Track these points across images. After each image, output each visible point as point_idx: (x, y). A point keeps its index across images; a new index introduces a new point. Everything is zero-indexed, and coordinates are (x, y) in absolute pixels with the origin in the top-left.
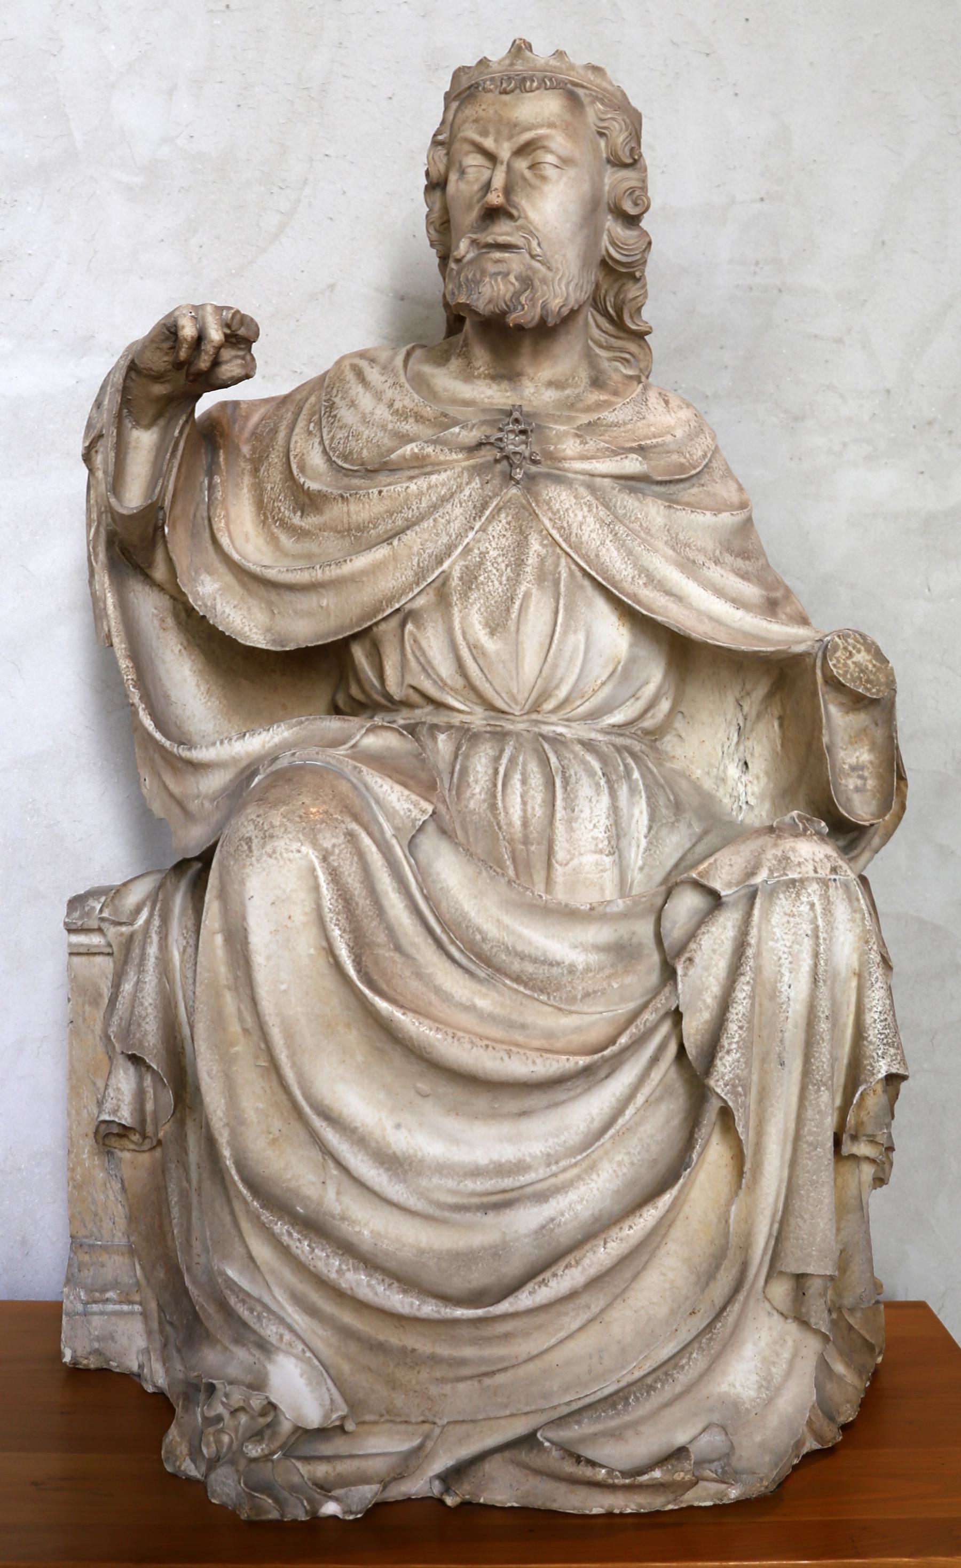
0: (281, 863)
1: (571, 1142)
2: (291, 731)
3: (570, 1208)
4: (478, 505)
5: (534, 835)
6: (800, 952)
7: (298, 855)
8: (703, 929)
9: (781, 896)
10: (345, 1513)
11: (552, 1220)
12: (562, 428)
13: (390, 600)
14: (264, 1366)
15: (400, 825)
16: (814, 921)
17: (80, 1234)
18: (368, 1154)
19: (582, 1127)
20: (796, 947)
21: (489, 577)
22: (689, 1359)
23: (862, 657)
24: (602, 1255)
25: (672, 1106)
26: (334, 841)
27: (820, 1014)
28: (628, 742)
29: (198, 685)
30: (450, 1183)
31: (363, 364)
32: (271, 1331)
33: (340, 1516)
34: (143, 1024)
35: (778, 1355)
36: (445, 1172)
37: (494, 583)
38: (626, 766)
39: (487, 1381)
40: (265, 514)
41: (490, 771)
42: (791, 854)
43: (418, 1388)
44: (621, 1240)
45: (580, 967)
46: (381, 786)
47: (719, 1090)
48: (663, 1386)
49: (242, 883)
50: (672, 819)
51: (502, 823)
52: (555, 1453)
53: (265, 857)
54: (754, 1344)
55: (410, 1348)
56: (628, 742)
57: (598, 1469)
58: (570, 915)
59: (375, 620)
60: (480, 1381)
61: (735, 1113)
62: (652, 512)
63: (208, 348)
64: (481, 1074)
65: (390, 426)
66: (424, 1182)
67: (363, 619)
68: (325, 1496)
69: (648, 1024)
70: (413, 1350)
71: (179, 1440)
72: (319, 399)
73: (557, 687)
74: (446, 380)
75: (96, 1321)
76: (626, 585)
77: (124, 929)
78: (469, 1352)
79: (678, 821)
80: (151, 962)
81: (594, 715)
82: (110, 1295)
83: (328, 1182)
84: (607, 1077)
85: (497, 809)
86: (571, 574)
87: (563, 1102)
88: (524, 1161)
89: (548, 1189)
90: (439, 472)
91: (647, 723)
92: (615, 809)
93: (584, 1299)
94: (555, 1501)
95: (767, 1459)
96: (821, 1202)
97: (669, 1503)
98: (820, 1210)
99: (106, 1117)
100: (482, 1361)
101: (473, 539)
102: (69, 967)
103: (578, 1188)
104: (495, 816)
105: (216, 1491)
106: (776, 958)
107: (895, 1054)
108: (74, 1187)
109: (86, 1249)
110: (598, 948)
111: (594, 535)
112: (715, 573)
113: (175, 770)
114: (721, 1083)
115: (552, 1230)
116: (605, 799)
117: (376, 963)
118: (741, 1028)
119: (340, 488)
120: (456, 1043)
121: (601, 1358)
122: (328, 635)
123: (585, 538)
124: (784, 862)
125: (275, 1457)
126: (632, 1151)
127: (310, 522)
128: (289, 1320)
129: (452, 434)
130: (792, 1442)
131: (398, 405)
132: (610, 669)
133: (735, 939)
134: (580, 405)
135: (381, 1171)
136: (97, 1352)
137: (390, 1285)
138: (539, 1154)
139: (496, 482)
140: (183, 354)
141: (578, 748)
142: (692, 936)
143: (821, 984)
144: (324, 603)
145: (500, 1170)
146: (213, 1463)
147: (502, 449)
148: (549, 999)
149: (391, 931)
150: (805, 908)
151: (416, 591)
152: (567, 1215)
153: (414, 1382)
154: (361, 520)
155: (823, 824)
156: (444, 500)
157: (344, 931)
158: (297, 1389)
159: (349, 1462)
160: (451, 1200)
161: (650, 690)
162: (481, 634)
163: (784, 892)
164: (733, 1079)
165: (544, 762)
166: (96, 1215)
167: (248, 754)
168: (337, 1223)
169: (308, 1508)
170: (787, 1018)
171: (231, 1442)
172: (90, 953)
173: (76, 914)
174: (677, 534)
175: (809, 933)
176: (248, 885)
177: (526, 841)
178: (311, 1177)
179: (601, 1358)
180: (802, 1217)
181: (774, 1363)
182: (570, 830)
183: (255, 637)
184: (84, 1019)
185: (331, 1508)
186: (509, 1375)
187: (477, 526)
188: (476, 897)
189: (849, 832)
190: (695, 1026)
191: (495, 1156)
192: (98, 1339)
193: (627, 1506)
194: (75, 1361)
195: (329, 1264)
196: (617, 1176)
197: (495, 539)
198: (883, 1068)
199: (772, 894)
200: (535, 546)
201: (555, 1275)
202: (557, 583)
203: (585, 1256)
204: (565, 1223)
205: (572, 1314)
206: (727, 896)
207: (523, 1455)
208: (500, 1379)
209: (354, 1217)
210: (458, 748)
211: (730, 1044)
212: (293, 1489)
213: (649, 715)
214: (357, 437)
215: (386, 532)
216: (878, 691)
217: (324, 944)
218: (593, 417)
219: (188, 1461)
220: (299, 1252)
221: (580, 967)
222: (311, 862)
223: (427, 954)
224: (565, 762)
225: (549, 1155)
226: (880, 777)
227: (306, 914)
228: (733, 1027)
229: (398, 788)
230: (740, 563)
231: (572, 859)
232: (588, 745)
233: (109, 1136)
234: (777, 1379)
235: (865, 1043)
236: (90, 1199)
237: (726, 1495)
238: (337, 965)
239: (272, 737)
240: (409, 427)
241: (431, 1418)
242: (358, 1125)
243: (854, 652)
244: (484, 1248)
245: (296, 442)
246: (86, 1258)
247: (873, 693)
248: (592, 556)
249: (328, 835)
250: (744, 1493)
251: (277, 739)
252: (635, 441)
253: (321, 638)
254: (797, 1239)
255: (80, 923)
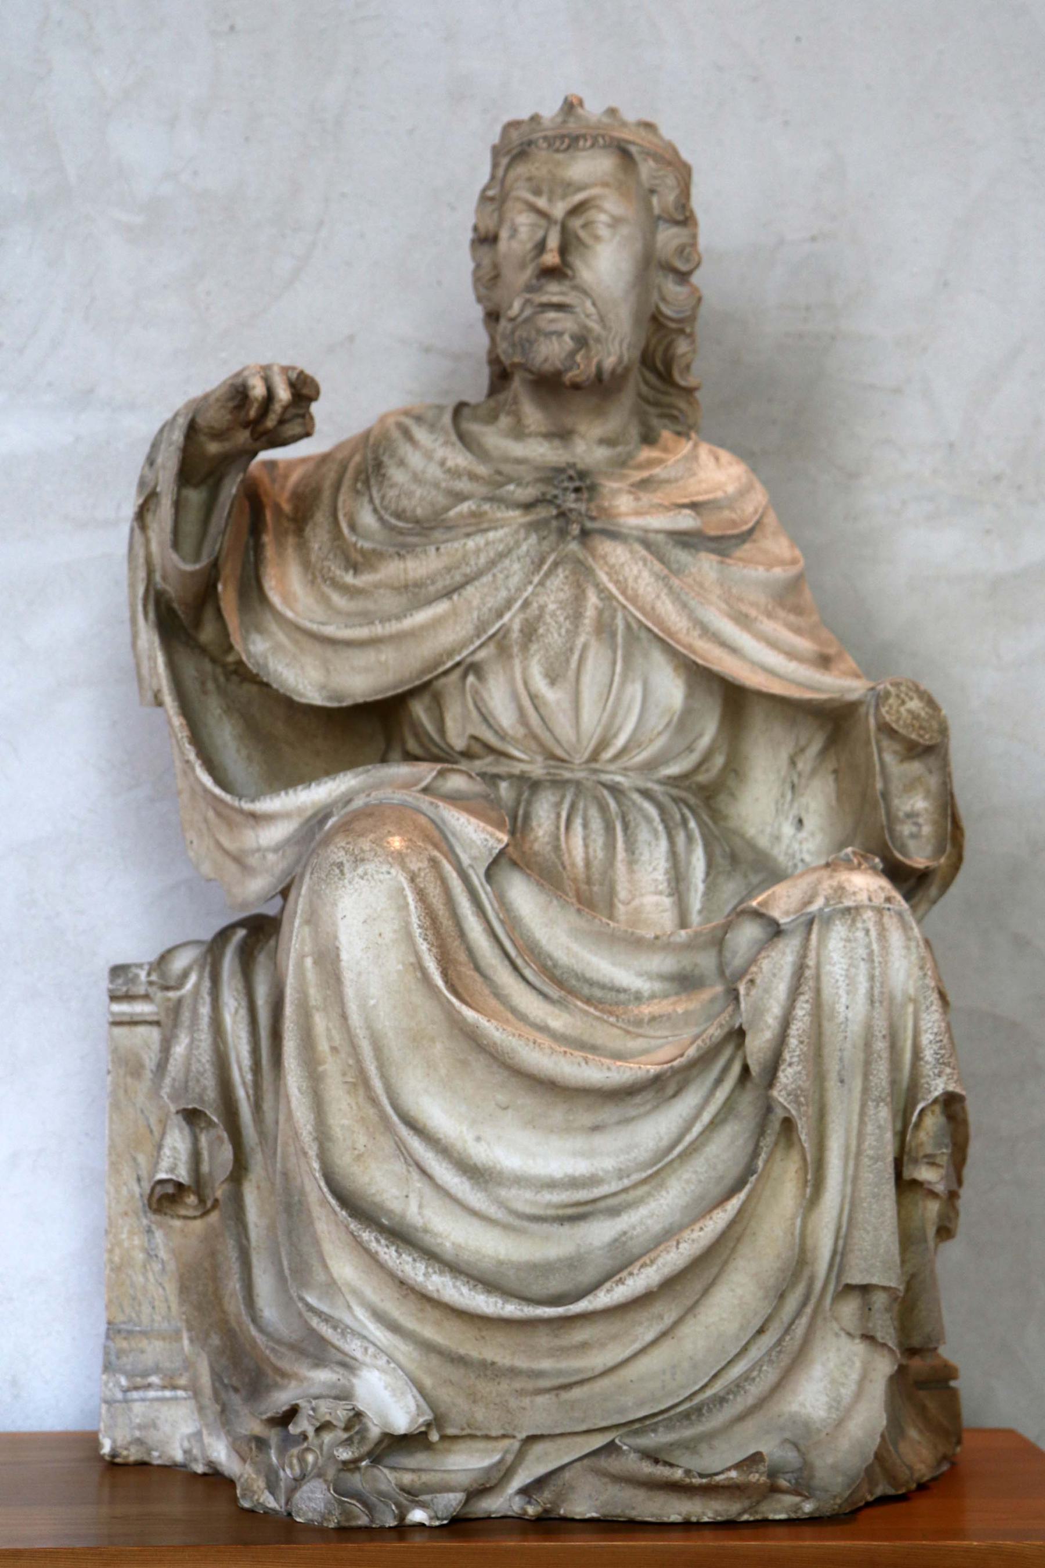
0: (373, 883)
1: (642, 1159)
2: (358, 779)
3: (641, 1223)
4: (536, 560)
5: (596, 876)
6: (857, 975)
7: (388, 876)
8: (763, 954)
9: (837, 922)
10: (431, 1518)
11: (625, 1233)
12: (615, 485)
13: (450, 654)
14: (349, 1380)
15: (478, 854)
16: (869, 946)
17: (117, 1321)
18: (451, 1163)
19: (651, 1145)
20: (853, 970)
21: (548, 630)
22: (760, 1371)
23: (915, 704)
24: (673, 1258)
25: (736, 1128)
26: (420, 865)
27: (877, 1033)
28: (683, 794)
29: (238, 751)
30: (529, 1195)
31: (408, 422)
32: (354, 1347)
33: (427, 1523)
34: (202, 1079)
35: (846, 1376)
36: (522, 1184)
37: (553, 636)
38: (683, 816)
39: (565, 1396)
40: (313, 574)
41: (553, 816)
42: (846, 885)
43: (498, 1400)
44: (693, 1241)
45: (646, 994)
46: (458, 819)
47: (781, 1100)
48: (735, 1397)
49: (335, 904)
50: (729, 868)
51: (567, 863)
52: (633, 1456)
53: (357, 879)
54: (823, 1365)
55: (489, 1361)
56: (683, 794)
57: (675, 1469)
58: (636, 944)
59: (435, 673)
60: (557, 1395)
61: (799, 1122)
62: (705, 566)
63: (277, 407)
64: (559, 1079)
65: (443, 485)
66: (503, 1193)
67: (423, 672)
68: (412, 1501)
69: (713, 1039)
70: (493, 1363)
71: (254, 1476)
72: (368, 462)
73: (615, 736)
74: (494, 438)
75: (138, 1408)
76: (682, 636)
77: (172, 995)
78: (546, 1364)
79: (734, 870)
80: (205, 1022)
81: (649, 766)
82: (154, 1379)
83: (411, 1195)
84: (675, 1095)
85: (560, 850)
86: (628, 627)
87: (633, 1119)
88: (597, 1175)
89: (620, 1204)
90: (495, 528)
91: (702, 778)
92: (673, 853)
93: (658, 1307)
94: (633, 1508)
95: (840, 1479)
96: (883, 1214)
97: (744, 1512)
98: (883, 1223)
99: (162, 1176)
100: (560, 1373)
101: (533, 593)
102: (111, 1038)
103: (648, 1203)
104: (559, 857)
105: (301, 1509)
106: (833, 981)
107: (952, 1074)
108: (112, 1270)
109: (124, 1335)
110: (662, 977)
111: (649, 589)
112: (768, 626)
113: (230, 824)
114: (783, 1093)
115: (624, 1243)
116: (664, 844)
117: (460, 978)
118: (802, 1042)
119: (395, 545)
120: (537, 1049)
121: (674, 1374)
122: (388, 689)
123: (641, 591)
124: (840, 892)
125: (364, 1463)
126: (699, 1169)
127: (364, 580)
128: (372, 1338)
129: (508, 492)
130: (864, 1466)
131: (450, 463)
132: (666, 720)
133: (794, 963)
134: (632, 463)
135: (464, 1179)
136: (139, 1442)
137: (475, 1286)
138: (610, 1168)
139: (553, 538)
140: (253, 413)
141: (636, 796)
142: (753, 961)
143: (877, 1005)
144: (383, 658)
145: (574, 1183)
146: (292, 1491)
147: (558, 506)
148: (618, 1021)
149: (470, 952)
150: (860, 934)
151: (478, 643)
152: (638, 1230)
153: (494, 1394)
154: (418, 576)
155: (877, 860)
156: (502, 556)
157: (433, 945)
158: (389, 1401)
159: (433, 1473)
160: (529, 1210)
161: (705, 741)
162: (540, 684)
163: (840, 919)
164: (795, 1090)
165: (603, 809)
166: (134, 1299)
167: (313, 804)
168: (420, 1235)
169: (396, 1512)
170: (846, 1037)
171: (317, 1459)
172: (133, 1022)
173: (120, 981)
174: (730, 588)
175: (865, 956)
176: (341, 905)
177: (589, 881)
178: (394, 1191)
179: (674, 1374)
180: (865, 1229)
181: (843, 1384)
182: (631, 871)
183: (310, 694)
184: (126, 1091)
185: (418, 1516)
186: (586, 1388)
187: (536, 579)
188: (547, 926)
189: (906, 880)
190: (758, 1044)
191: (570, 1171)
192: (140, 1427)
193: (704, 1514)
194: (114, 1455)
195: (415, 1270)
196: (686, 1193)
197: (555, 593)
198: (938, 1087)
199: (827, 921)
200: (593, 599)
201: (631, 1274)
202: (613, 635)
203: (659, 1256)
204: (638, 1236)
205: (645, 1324)
206: (785, 924)
207: (604, 1463)
208: (576, 1393)
209: (436, 1230)
210: (520, 794)
211: (791, 1057)
212: (381, 1494)
213: (704, 768)
214: (410, 495)
215: (445, 587)
216: (931, 738)
217: (412, 959)
218: (645, 474)
219: (267, 1493)
220: (387, 1257)
221: (646, 994)
222: (400, 882)
223: (504, 976)
224: (625, 808)
225: (620, 1170)
226: (935, 823)
227: (395, 931)
228: (793, 1042)
229: (473, 820)
230: (792, 618)
231: (633, 899)
232: (646, 794)
233: (166, 1199)
234: (846, 1401)
235: (922, 1063)
236: (128, 1282)
237: (800, 1508)
238: (425, 978)
239: (339, 786)
240: (463, 485)
241: (510, 1432)
242: (441, 1136)
243: (907, 699)
244: (560, 1260)
245: (344, 501)
246: (124, 1344)
247: (927, 739)
248: (648, 608)
249: (414, 859)
250: (817, 1509)
251: (343, 788)
252: (685, 497)
253: (381, 692)
254: (860, 1250)
255: (124, 989)
